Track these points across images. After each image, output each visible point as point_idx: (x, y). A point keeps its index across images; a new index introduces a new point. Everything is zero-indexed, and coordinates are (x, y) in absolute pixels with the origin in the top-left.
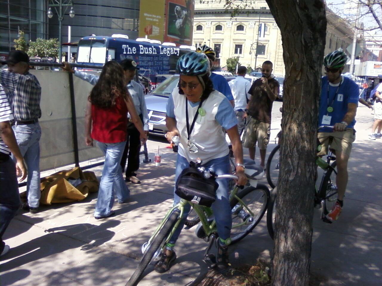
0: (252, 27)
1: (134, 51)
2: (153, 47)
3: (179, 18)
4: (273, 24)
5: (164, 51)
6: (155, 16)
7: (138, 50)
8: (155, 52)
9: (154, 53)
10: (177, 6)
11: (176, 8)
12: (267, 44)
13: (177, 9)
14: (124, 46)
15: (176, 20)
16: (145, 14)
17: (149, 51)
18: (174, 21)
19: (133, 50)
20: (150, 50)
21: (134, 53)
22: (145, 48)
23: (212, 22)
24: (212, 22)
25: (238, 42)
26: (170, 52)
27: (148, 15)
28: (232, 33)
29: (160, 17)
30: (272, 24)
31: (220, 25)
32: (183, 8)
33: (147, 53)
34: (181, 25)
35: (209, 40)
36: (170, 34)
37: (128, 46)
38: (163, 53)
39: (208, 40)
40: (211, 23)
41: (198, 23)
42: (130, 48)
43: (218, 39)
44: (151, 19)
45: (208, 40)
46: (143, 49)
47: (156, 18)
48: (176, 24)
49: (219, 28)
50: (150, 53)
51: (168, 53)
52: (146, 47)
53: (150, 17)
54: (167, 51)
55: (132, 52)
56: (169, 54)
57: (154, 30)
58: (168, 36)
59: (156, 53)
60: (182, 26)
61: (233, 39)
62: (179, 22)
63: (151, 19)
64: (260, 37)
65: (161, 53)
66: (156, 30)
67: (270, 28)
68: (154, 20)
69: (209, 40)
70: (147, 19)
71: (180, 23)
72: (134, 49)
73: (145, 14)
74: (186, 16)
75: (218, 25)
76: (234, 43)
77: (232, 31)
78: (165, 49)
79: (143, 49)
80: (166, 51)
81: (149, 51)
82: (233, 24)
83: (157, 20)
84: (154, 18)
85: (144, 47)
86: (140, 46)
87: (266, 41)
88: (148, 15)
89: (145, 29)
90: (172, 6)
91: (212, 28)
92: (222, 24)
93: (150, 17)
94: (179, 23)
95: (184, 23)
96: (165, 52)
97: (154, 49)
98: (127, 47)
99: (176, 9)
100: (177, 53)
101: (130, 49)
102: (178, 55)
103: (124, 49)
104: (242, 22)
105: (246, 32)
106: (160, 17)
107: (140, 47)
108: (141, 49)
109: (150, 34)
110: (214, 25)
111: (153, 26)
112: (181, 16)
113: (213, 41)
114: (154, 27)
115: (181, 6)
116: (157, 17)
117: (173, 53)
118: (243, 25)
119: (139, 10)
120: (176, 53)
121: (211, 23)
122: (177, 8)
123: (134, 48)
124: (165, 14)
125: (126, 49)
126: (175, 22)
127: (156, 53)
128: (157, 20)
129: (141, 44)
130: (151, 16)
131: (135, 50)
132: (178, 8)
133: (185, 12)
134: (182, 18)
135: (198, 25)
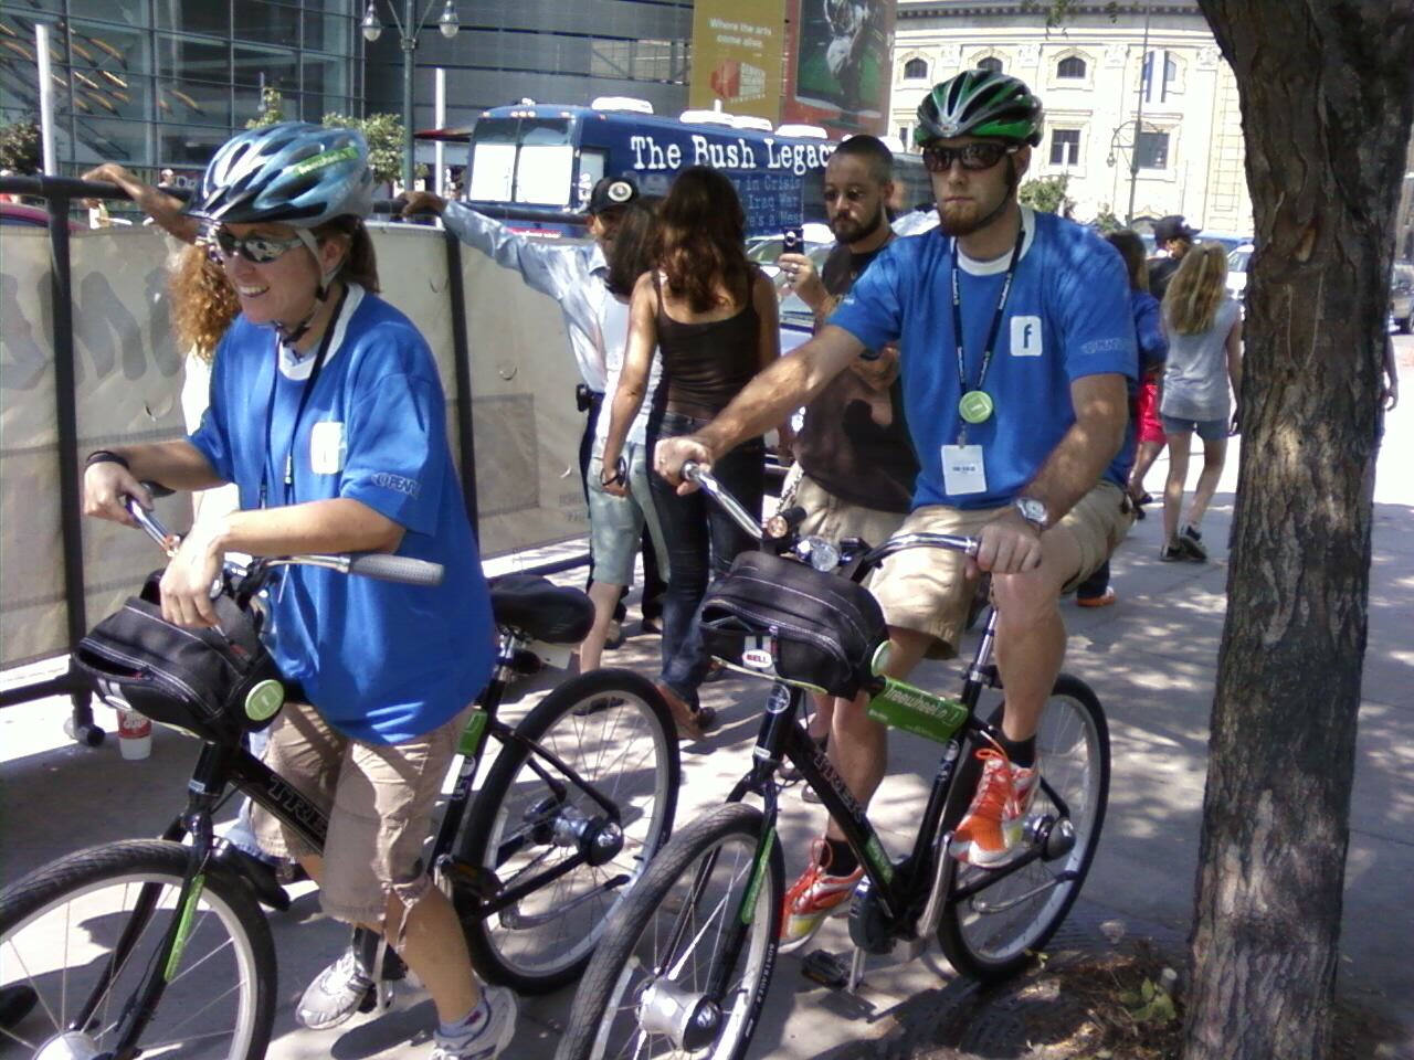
0: (1029, 64)
1: (674, 160)
2: (742, 142)
3: (840, 33)
4: (1198, 54)
5: (784, 156)
6: (750, 29)
7: (688, 152)
8: (748, 161)
9: (745, 165)
12: (1173, 126)
14: (637, 141)
15: (829, 41)
16: (714, 23)
17: (726, 158)
18: (821, 44)
19: (670, 155)
20: (730, 154)
21: (674, 166)
22: (712, 147)
24: (962, 46)
26: (805, 159)
27: (726, 26)
30: (1195, 50)
33: (722, 164)
34: (845, 60)
36: (803, 92)
37: (650, 140)
38: (778, 166)
42: (658, 149)
46: (704, 150)
47: (754, 36)
48: (829, 55)
50: (731, 164)
51: (796, 164)
52: (715, 144)
53: (730, 33)
54: (793, 158)
55: (666, 161)
56: (800, 168)
57: (744, 79)
58: (798, 99)
59: (753, 165)
60: (850, 62)
62: (839, 48)
64: (1148, 100)
65: (772, 165)
66: (753, 80)
68: (748, 42)
70: (720, 39)
71: (842, 52)
72: (674, 151)
73: (714, 23)
74: (867, 24)
75: (987, 56)
78: (785, 148)
79: (704, 150)
80: (789, 155)
81: (726, 158)
83: (758, 44)
84: (743, 35)
85: (709, 143)
86: (696, 139)
87: (1172, 115)
88: (726, 26)
89: (715, 77)
93: (730, 33)
94: (838, 50)
95: (858, 51)
96: (787, 160)
97: (746, 150)
98: (647, 144)
101: (656, 153)
103: (635, 152)
104: (1079, 47)
107: (693, 145)
108: (698, 150)
109: (731, 95)
112: (847, 25)
114: (744, 68)
116: (759, 31)
117: (816, 164)
118: (1084, 59)
119: (692, 7)
123: (673, 147)
124: (787, 21)
125: (646, 152)
127: (753, 165)
128: (758, 44)
129: (698, 134)
130: (736, 27)
131: (678, 155)
133: (861, 13)
134: (851, 35)
135: (1064, 57)
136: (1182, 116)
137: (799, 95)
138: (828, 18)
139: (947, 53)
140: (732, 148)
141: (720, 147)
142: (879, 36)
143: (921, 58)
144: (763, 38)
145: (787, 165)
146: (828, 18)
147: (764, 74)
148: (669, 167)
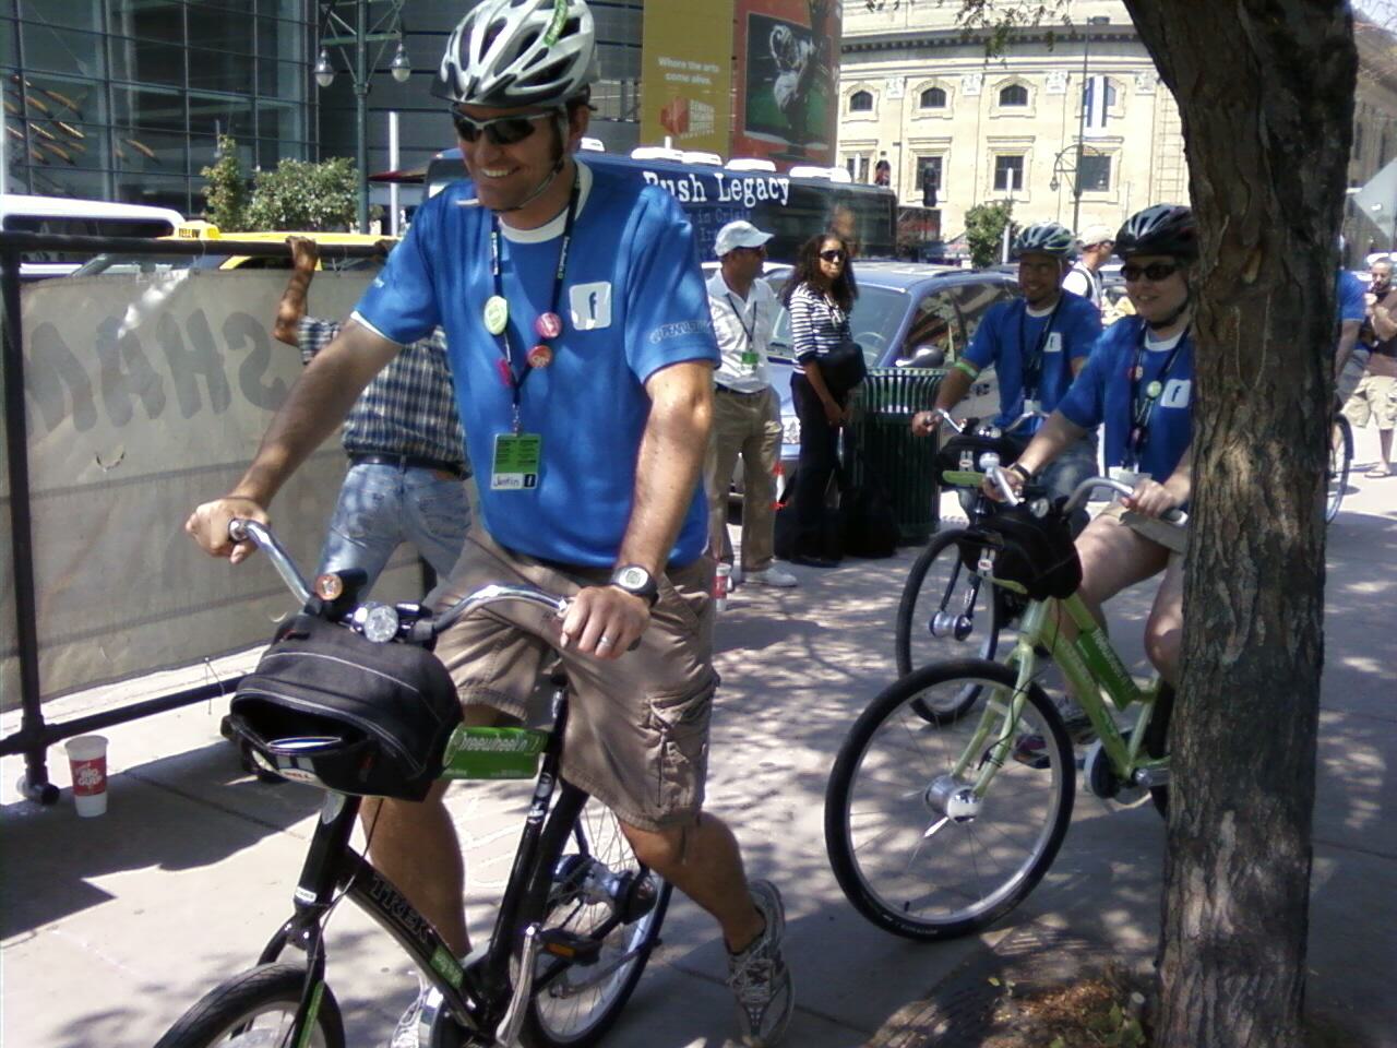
0: (972, 93)
2: (692, 176)
3: (787, 69)
4: (1136, 79)
5: (734, 189)
6: (698, 67)
8: (699, 195)
9: (696, 199)
10: (778, 28)
11: (773, 34)
13: (779, 36)
15: (776, 76)
16: (663, 62)
20: (681, 189)
23: (906, 78)
24: (906, 78)
25: (1008, 148)
26: (754, 192)
28: (985, 117)
29: (715, 69)
30: (1132, 76)
31: (938, 86)
32: (799, 34)
34: (792, 94)
35: (899, 144)
38: (728, 199)
39: (895, 144)
40: (905, 83)
41: (855, 83)
43: (929, 140)
44: (686, 79)
45: (895, 144)
47: (702, 73)
49: (933, 98)
51: (746, 197)
54: (743, 191)
56: (750, 201)
57: (693, 116)
58: (747, 134)
59: (703, 199)
60: (797, 96)
61: (988, 138)
63: (686, 79)
64: (1089, 124)
65: (722, 199)
66: (703, 116)
67: (1124, 94)
68: (697, 80)
69: (899, 144)
70: (669, 77)
71: (788, 87)
73: (663, 62)
74: (812, 59)
75: (931, 86)
76: (993, 149)
77: (908, 107)
78: (735, 182)
80: (739, 188)
82: (986, 82)
83: (707, 81)
84: (692, 73)
85: (659, 179)
89: (664, 113)
90: (759, 28)
91: (908, 100)
92: (944, 83)
94: (785, 85)
95: (805, 85)
96: (737, 193)
97: (696, 184)
99: (775, 37)
100: (782, 196)
102: (784, 202)
104: (1021, 76)
105: (877, 114)
106: (715, 69)
109: (681, 131)
110: (847, 92)
111: (692, 102)
112: (792, 60)
113: (993, 145)
115: (789, 26)
116: (707, 68)
117: (766, 196)
119: (640, 46)
120: (775, 196)
121: (905, 83)
122: (779, 32)
126: (773, 83)
127: (703, 199)
128: (707, 81)
130: (684, 65)
132: (782, 33)
133: (806, 48)
134: (797, 70)
135: (1006, 84)
136: (1123, 139)
137: (747, 129)
138: (774, 54)
139: (891, 85)
140: (683, 183)
141: (671, 183)
142: (824, 70)
143: (867, 90)
144: (710, 75)
145: (737, 198)
146: (774, 54)
147: (712, 110)
148: (770, 198)
